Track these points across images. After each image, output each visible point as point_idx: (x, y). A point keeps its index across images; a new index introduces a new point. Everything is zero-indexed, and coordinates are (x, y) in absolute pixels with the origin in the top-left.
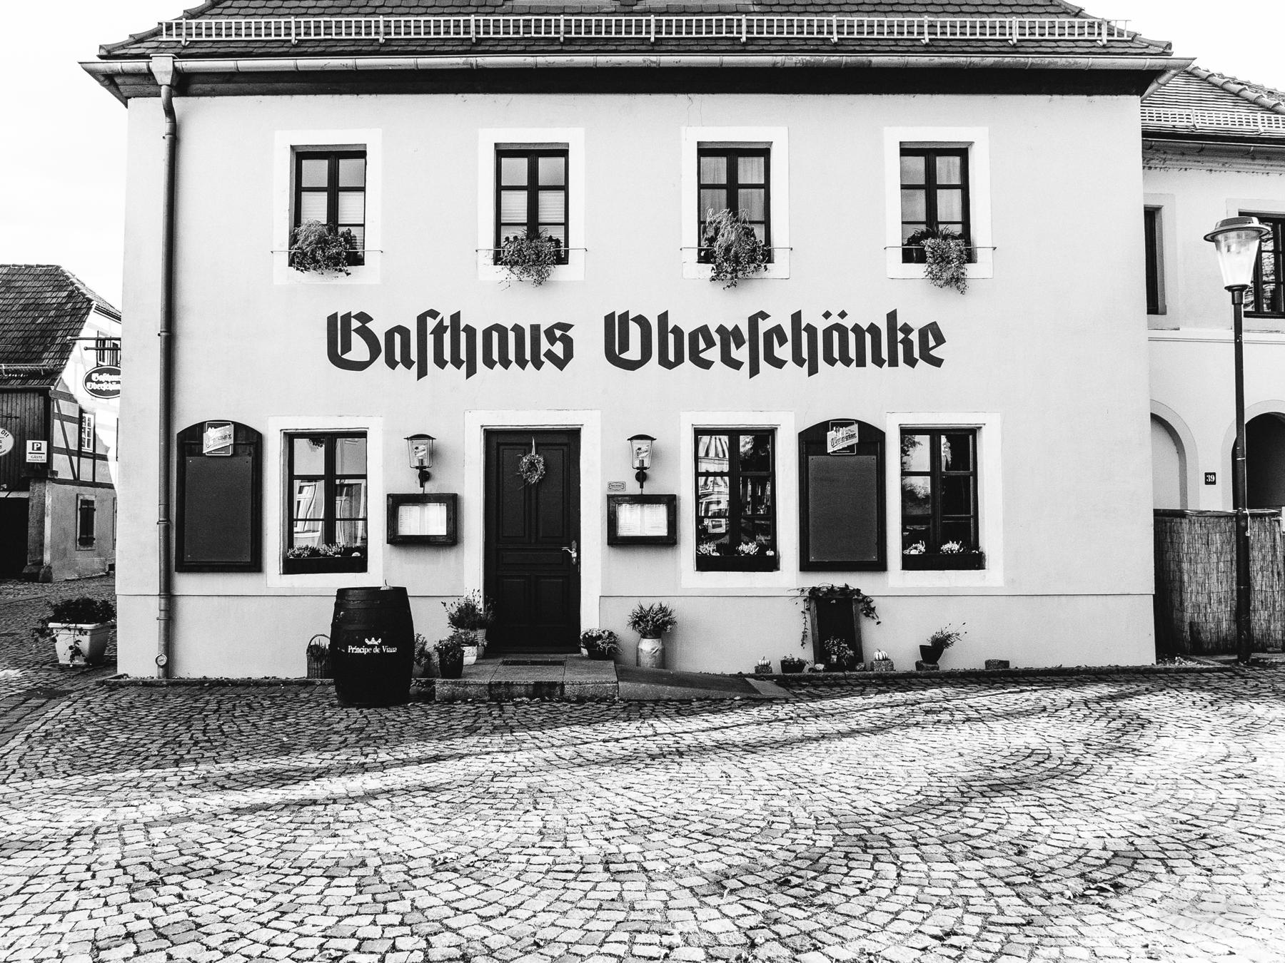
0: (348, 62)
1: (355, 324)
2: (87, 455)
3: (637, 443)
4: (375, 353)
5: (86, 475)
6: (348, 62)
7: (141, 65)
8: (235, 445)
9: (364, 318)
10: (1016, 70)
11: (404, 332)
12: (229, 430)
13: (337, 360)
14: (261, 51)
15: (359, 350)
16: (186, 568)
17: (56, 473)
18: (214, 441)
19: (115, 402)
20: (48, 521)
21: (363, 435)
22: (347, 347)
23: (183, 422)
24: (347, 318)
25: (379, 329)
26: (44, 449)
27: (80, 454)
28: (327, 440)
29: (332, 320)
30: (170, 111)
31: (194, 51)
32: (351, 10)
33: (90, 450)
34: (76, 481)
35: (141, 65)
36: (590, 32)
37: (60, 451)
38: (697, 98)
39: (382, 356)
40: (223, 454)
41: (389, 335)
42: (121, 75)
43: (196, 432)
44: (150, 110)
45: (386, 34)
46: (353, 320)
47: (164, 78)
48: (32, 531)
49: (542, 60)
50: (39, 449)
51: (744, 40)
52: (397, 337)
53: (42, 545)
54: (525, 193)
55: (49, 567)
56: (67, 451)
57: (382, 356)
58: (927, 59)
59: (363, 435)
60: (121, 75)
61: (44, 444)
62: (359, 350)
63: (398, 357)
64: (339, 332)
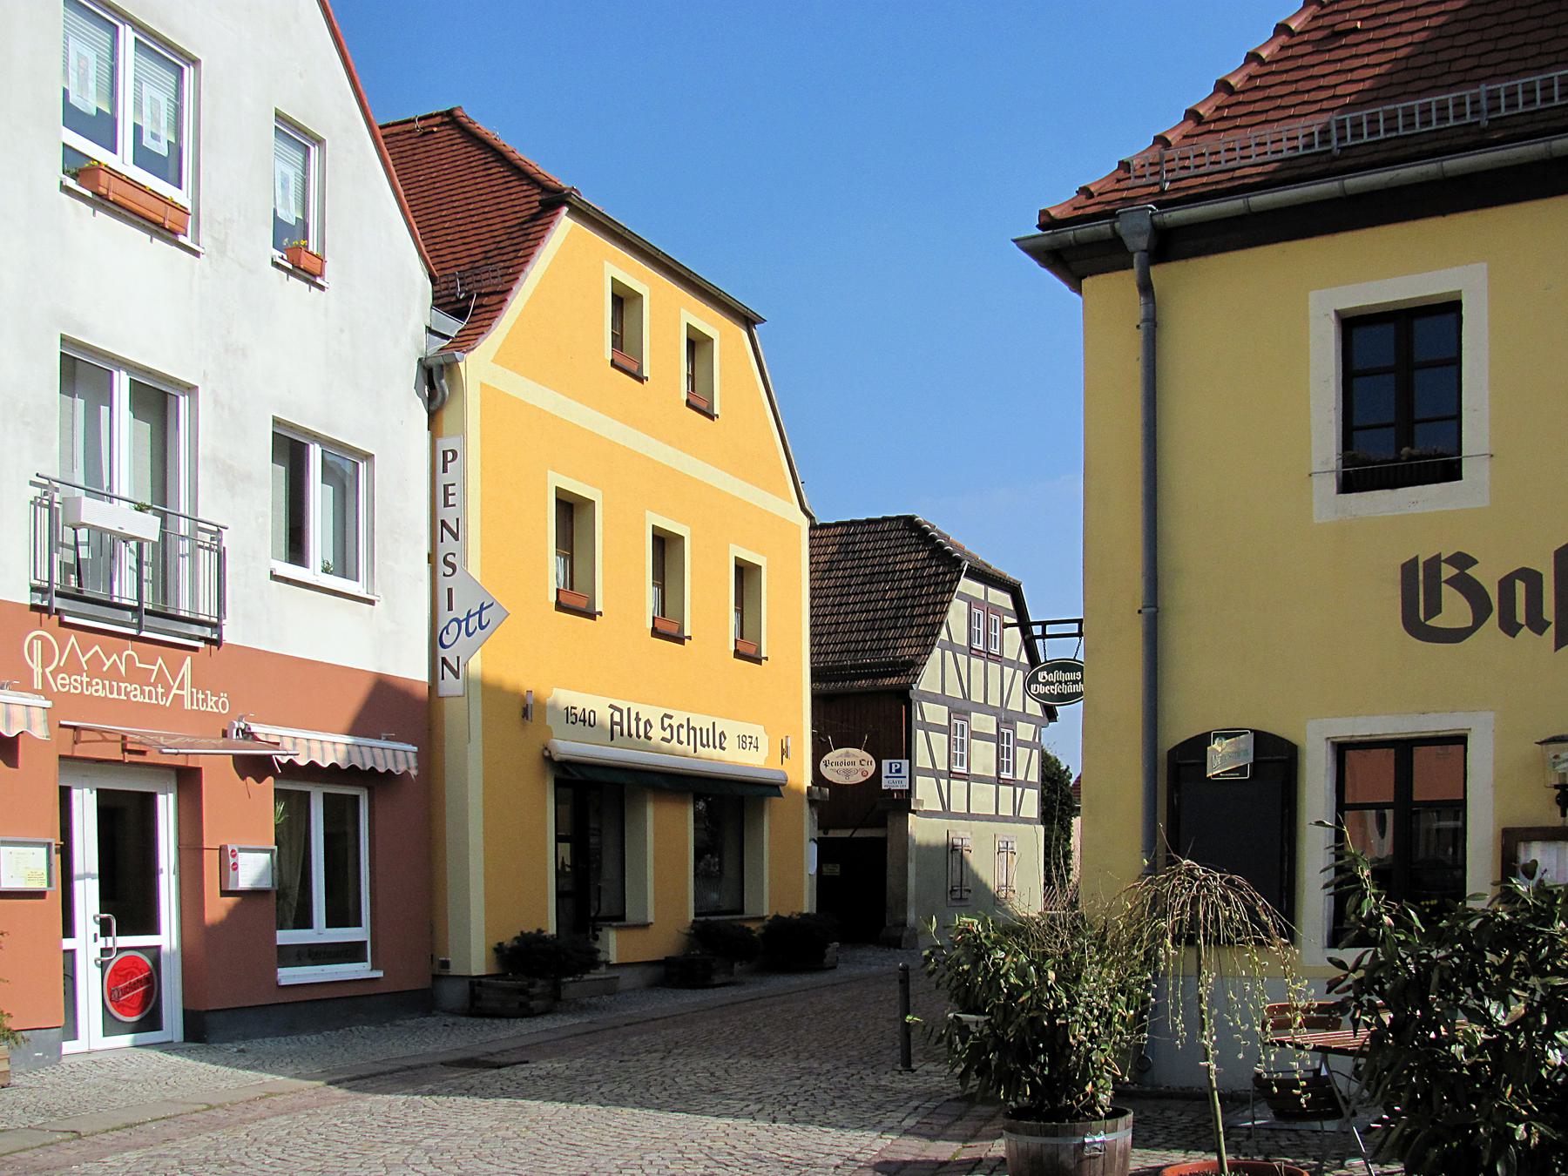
0: (1428, 168)
1: (1448, 571)
2: (1007, 782)
3: (1553, 748)
4: (1481, 610)
5: (958, 805)
6: (1428, 168)
7: (1103, 227)
8: (1254, 765)
9: (1463, 561)
10: (1507, 168)
11: (1532, 579)
12: (1247, 742)
13: (1416, 627)
14: (1314, 170)
15: (1455, 610)
16: (622, 918)
17: (920, 802)
18: (1222, 758)
19: (1079, 705)
20: (912, 867)
21: (1461, 740)
22: (1434, 608)
23: (1177, 732)
24: (1434, 564)
25: (1487, 576)
26: (905, 771)
27: (951, 775)
28: (1404, 749)
29: (1409, 569)
30: (1146, 288)
31: (1350, 162)
32: (1450, 79)
33: (1009, 776)
34: (946, 812)
35: (1103, 227)
36: (1429, 123)
37: (925, 772)
38: (1480, 212)
39: (1494, 617)
40: (1236, 777)
41: (1506, 585)
42: (1074, 248)
43: (1199, 744)
44: (1115, 290)
45: (1490, 111)
46: (1444, 566)
47: (1139, 243)
48: (891, 881)
49: (1355, 182)
50: (898, 771)
51: (1337, 152)
52: (1520, 587)
53: (905, 900)
54: (1390, 379)
55: (914, 929)
56: (934, 773)
57: (1494, 617)
58: (1541, 146)
59: (1461, 740)
60: (1074, 248)
61: (905, 763)
62: (1455, 610)
63: (1521, 617)
64: (1421, 589)
